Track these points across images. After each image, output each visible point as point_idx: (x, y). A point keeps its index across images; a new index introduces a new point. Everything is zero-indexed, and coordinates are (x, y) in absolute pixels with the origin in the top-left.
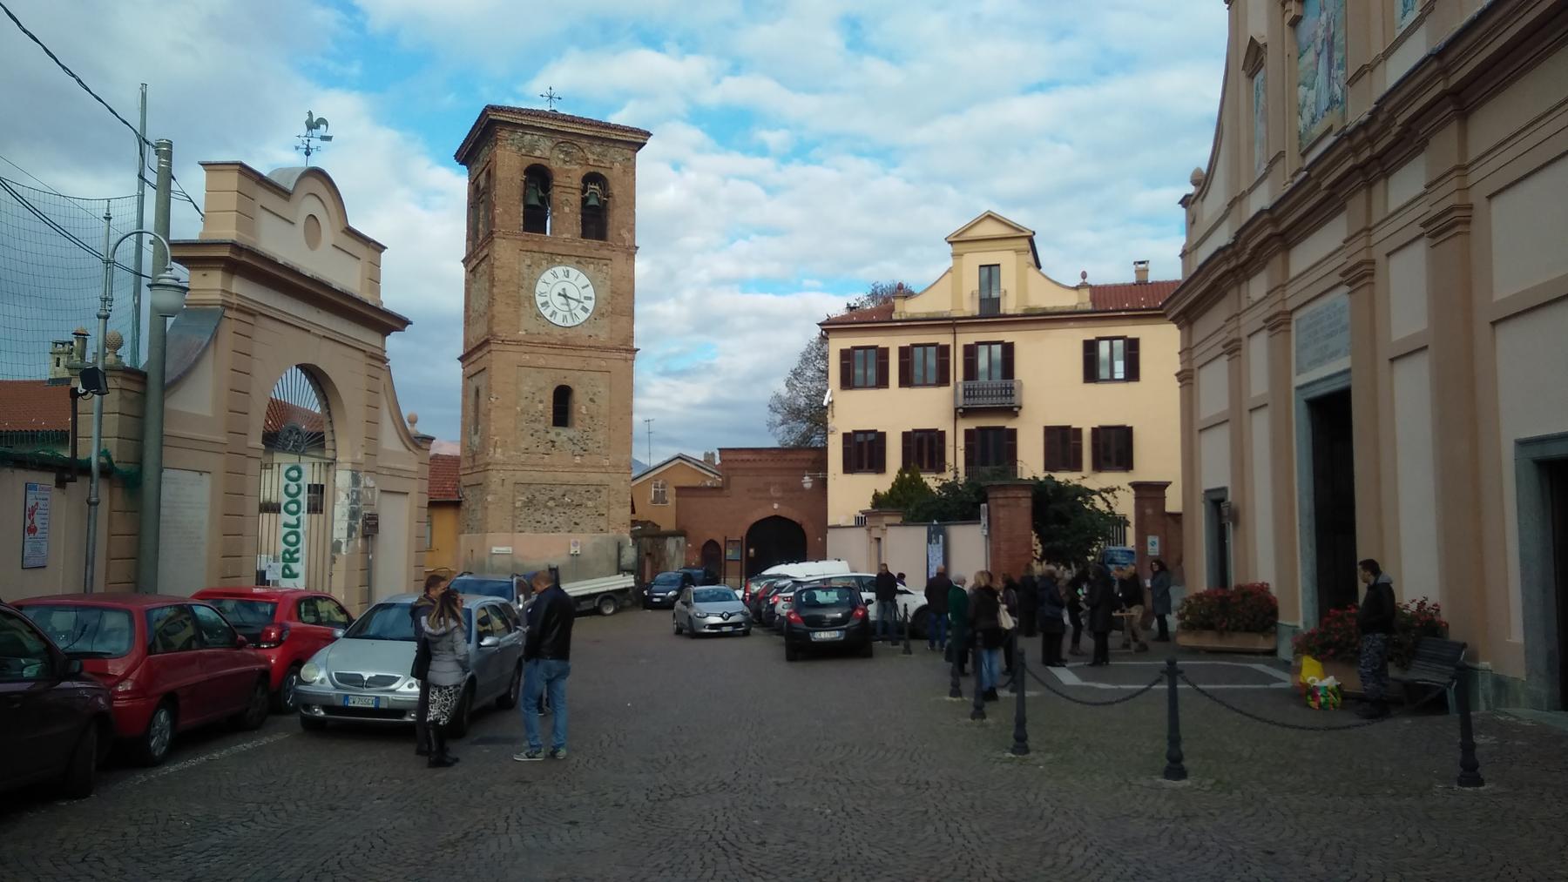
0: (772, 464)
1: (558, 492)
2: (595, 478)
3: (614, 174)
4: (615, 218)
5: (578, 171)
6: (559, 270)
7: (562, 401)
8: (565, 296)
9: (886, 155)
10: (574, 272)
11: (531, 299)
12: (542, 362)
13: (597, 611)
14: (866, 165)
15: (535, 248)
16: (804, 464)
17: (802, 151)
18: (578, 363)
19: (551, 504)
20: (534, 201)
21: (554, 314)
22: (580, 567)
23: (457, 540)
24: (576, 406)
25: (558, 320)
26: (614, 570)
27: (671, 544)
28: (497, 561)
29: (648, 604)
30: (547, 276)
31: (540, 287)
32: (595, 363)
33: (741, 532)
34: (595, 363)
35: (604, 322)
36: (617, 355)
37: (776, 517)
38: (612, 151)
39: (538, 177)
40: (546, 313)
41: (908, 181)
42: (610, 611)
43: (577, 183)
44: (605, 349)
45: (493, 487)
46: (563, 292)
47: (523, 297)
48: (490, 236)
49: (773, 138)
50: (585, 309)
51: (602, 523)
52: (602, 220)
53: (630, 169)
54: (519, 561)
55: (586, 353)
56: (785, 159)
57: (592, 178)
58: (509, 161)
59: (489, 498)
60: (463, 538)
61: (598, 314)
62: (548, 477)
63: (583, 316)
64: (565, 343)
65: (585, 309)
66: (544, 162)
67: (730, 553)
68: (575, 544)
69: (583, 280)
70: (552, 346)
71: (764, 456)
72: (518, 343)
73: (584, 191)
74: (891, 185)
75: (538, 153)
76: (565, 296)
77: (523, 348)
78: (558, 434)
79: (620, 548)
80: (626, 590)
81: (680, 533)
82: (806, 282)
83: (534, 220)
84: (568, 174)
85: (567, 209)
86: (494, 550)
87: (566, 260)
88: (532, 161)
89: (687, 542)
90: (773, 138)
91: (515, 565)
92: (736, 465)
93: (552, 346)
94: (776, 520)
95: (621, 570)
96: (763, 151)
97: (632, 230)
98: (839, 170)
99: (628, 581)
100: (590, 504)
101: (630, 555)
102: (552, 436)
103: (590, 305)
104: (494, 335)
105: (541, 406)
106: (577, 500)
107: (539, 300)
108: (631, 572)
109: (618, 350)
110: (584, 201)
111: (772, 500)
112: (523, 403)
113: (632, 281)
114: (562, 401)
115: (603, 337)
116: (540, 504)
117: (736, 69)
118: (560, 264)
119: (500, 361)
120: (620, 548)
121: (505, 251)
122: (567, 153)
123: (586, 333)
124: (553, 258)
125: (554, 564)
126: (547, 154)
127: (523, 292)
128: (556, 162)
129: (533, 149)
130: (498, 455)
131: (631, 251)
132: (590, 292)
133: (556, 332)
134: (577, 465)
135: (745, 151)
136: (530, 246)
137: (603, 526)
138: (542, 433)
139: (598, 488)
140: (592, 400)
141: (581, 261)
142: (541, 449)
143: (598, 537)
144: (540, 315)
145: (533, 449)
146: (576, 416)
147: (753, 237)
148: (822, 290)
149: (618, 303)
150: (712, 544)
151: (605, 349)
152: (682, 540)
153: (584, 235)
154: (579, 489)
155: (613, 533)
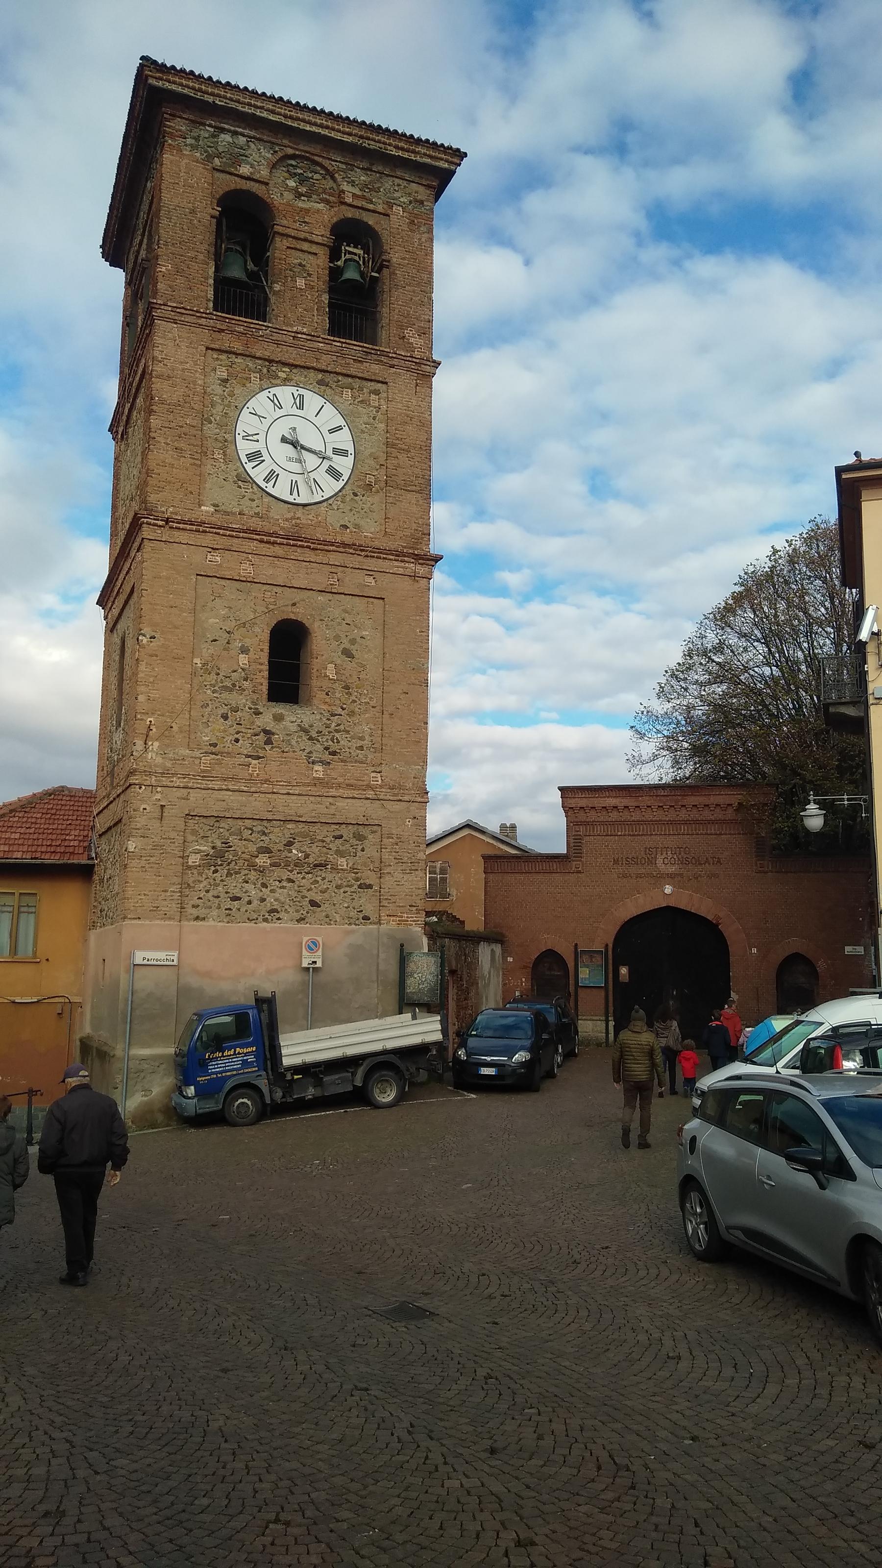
0: (659, 815)
1: (277, 836)
2: (352, 809)
3: (393, 227)
4: (393, 306)
5: (320, 217)
6: (285, 393)
7: (288, 646)
8: (295, 444)
9: (626, 594)
10: (313, 400)
11: (228, 444)
12: (246, 570)
13: (360, 1097)
14: (607, 603)
15: (238, 346)
16: (718, 814)
17: (544, 589)
18: (321, 579)
19: (262, 860)
20: (236, 272)
21: (272, 476)
22: (324, 1000)
23: (86, 940)
24: (316, 664)
25: (281, 490)
26: (392, 999)
27: (485, 953)
28: (145, 982)
29: (466, 1078)
30: (261, 402)
31: (246, 423)
32: (353, 580)
33: (603, 936)
34: (353, 580)
35: (374, 501)
36: (395, 566)
37: (668, 908)
38: (388, 183)
39: (244, 222)
40: (258, 474)
41: (649, 616)
42: (388, 1096)
43: (321, 233)
44: (379, 553)
45: (140, 821)
46: (291, 437)
47: (210, 438)
48: (149, 322)
49: (513, 579)
50: (334, 473)
51: (367, 903)
52: (367, 313)
53: (422, 223)
54: (194, 982)
55: (335, 558)
56: (525, 598)
57: (350, 232)
58: (187, 182)
59: (131, 846)
60: (93, 935)
61: (361, 485)
62: (256, 805)
63: (331, 487)
64: (293, 535)
65: (334, 473)
66: (255, 188)
67: (584, 974)
68: (313, 946)
69: (331, 416)
70: (267, 537)
71: (646, 800)
72: (199, 526)
73: (334, 254)
74: (630, 622)
75: (245, 170)
76: (295, 444)
77: (208, 540)
78: (278, 718)
79: (403, 959)
80: (421, 1049)
81: (493, 937)
82: (544, 714)
83: (242, 296)
84: (304, 215)
85: (301, 283)
86: (139, 957)
87: (297, 375)
88: (235, 184)
89: (505, 953)
90: (513, 579)
91: (184, 992)
92: (592, 816)
93: (267, 537)
94: (669, 915)
95: (406, 1003)
96: (503, 592)
97: (426, 332)
98: (578, 607)
99: (426, 1029)
100: (342, 862)
101: (424, 970)
102: (266, 720)
103: (345, 465)
104: (150, 512)
105: (243, 659)
106: (316, 853)
107: (244, 448)
108: (429, 1008)
109: (399, 555)
110: (335, 273)
111: (661, 878)
112: (207, 651)
113: (426, 425)
114: (288, 646)
115: (370, 530)
116: (239, 861)
117: (481, 514)
118: (286, 382)
119: (155, 560)
120: (403, 959)
121: (172, 345)
122: (302, 180)
123: (334, 519)
124: (273, 370)
125: (266, 990)
126: (264, 173)
127: (210, 430)
128: (281, 191)
129: (238, 158)
130: (154, 754)
131: (424, 369)
132: (344, 439)
133: (277, 512)
134: (318, 782)
135: (484, 592)
136: (226, 341)
137: (370, 909)
138: (244, 715)
139: (361, 829)
140: (347, 653)
141: (327, 381)
142: (244, 746)
143: (361, 933)
144: (244, 479)
145: (227, 744)
146: (315, 683)
147: (492, 671)
148: (559, 722)
149: (400, 466)
150: (550, 957)
151: (379, 553)
152: (498, 948)
153: (332, 331)
154: (322, 832)
155: (389, 926)
